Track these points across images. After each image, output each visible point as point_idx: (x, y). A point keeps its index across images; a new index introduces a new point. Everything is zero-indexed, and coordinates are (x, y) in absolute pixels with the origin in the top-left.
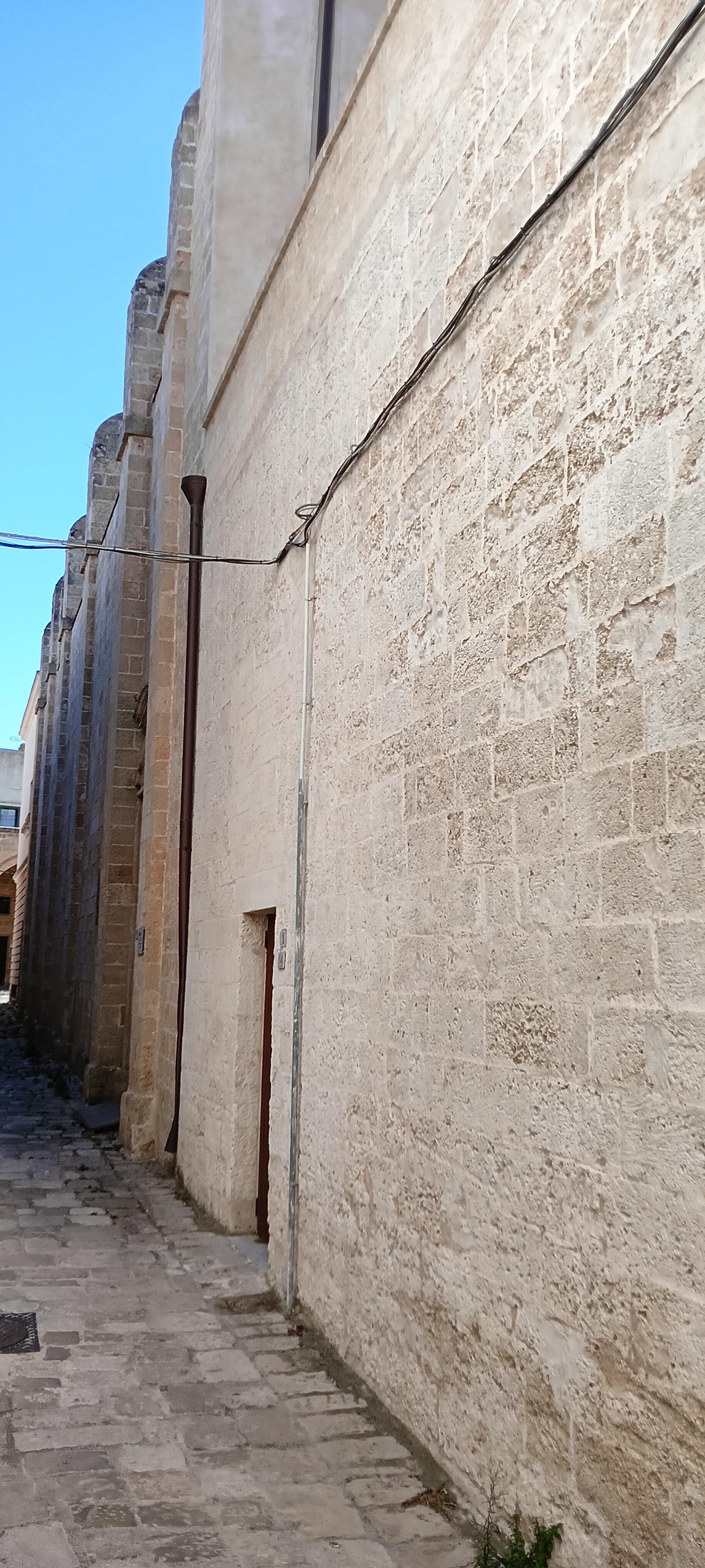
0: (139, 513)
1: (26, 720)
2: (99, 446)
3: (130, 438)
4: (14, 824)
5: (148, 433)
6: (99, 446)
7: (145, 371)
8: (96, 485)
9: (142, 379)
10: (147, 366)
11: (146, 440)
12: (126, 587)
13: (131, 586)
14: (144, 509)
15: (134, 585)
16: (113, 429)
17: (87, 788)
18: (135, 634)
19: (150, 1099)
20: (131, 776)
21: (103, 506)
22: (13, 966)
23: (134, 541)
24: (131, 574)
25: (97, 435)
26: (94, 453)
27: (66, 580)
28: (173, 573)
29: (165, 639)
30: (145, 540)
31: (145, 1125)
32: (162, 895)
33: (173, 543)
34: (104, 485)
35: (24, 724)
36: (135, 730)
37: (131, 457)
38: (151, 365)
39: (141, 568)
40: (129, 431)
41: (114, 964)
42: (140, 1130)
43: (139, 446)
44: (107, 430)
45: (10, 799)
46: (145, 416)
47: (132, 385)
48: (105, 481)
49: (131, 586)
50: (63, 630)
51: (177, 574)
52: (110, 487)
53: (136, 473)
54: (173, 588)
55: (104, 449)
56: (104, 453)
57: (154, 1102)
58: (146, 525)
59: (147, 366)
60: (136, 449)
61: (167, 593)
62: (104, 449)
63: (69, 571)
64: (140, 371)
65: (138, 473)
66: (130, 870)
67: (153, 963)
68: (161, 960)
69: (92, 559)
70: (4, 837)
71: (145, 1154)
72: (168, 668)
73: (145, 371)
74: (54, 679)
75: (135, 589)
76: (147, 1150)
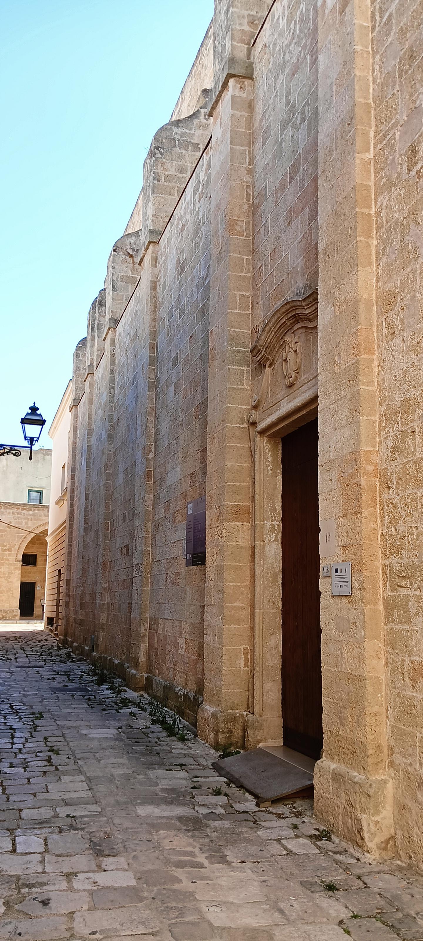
0: (243, 153)
1: (56, 421)
2: (157, 148)
3: (232, 82)
4: (39, 501)
5: (248, 76)
6: (157, 148)
7: (243, 17)
8: (156, 182)
9: (240, 24)
10: (246, 13)
11: (247, 82)
12: (231, 226)
13: (237, 224)
14: (247, 149)
15: (240, 223)
16: (169, 134)
17: (155, 448)
18: (242, 272)
19: (385, 782)
20: (243, 414)
21: (162, 200)
22: (46, 602)
23: (239, 179)
24: (237, 212)
25: (155, 138)
26: (151, 154)
27: (109, 288)
28: (368, 134)
29: (363, 210)
30: (249, 179)
31: (382, 816)
32: (376, 522)
33: (365, 98)
34: (162, 182)
35: (54, 425)
36: (245, 368)
37: (233, 97)
38: (249, 12)
39: (246, 207)
40: (232, 72)
41: (235, 604)
42: (377, 822)
43: (241, 88)
44: (164, 134)
45: (36, 485)
46: (245, 59)
47: (232, 30)
48: (163, 179)
49: (237, 224)
50: (109, 329)
51: (372, 134)
52: (168, 184)
53: (238, 113)
54: (368, 151)
55: (162, 150)
56: (162, 154)
57: (390, 785)
58: (250, 164)
59: (246, 13)
60: (238, 90)
61: (362, 156)
62: (162, 150)
63: (113, 281)
64: (238, 17)
65: (240, 114)
66: (35, 556)
67: (372, 606)
68: (381, 602)
69: (154, 246)
70: (34, 510)
71: (384, 853)
72: (368, 246)
73: (243, 17)
74: (92, 377)
75: (241, 227)
76: (385, 849)
